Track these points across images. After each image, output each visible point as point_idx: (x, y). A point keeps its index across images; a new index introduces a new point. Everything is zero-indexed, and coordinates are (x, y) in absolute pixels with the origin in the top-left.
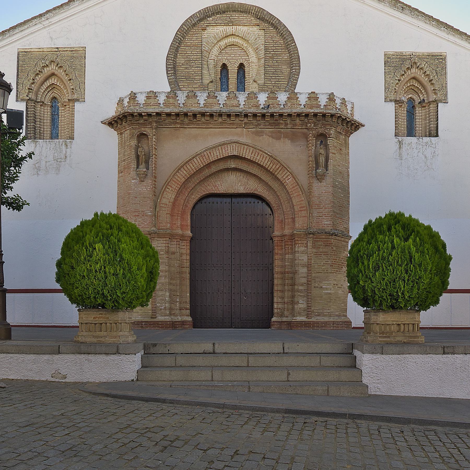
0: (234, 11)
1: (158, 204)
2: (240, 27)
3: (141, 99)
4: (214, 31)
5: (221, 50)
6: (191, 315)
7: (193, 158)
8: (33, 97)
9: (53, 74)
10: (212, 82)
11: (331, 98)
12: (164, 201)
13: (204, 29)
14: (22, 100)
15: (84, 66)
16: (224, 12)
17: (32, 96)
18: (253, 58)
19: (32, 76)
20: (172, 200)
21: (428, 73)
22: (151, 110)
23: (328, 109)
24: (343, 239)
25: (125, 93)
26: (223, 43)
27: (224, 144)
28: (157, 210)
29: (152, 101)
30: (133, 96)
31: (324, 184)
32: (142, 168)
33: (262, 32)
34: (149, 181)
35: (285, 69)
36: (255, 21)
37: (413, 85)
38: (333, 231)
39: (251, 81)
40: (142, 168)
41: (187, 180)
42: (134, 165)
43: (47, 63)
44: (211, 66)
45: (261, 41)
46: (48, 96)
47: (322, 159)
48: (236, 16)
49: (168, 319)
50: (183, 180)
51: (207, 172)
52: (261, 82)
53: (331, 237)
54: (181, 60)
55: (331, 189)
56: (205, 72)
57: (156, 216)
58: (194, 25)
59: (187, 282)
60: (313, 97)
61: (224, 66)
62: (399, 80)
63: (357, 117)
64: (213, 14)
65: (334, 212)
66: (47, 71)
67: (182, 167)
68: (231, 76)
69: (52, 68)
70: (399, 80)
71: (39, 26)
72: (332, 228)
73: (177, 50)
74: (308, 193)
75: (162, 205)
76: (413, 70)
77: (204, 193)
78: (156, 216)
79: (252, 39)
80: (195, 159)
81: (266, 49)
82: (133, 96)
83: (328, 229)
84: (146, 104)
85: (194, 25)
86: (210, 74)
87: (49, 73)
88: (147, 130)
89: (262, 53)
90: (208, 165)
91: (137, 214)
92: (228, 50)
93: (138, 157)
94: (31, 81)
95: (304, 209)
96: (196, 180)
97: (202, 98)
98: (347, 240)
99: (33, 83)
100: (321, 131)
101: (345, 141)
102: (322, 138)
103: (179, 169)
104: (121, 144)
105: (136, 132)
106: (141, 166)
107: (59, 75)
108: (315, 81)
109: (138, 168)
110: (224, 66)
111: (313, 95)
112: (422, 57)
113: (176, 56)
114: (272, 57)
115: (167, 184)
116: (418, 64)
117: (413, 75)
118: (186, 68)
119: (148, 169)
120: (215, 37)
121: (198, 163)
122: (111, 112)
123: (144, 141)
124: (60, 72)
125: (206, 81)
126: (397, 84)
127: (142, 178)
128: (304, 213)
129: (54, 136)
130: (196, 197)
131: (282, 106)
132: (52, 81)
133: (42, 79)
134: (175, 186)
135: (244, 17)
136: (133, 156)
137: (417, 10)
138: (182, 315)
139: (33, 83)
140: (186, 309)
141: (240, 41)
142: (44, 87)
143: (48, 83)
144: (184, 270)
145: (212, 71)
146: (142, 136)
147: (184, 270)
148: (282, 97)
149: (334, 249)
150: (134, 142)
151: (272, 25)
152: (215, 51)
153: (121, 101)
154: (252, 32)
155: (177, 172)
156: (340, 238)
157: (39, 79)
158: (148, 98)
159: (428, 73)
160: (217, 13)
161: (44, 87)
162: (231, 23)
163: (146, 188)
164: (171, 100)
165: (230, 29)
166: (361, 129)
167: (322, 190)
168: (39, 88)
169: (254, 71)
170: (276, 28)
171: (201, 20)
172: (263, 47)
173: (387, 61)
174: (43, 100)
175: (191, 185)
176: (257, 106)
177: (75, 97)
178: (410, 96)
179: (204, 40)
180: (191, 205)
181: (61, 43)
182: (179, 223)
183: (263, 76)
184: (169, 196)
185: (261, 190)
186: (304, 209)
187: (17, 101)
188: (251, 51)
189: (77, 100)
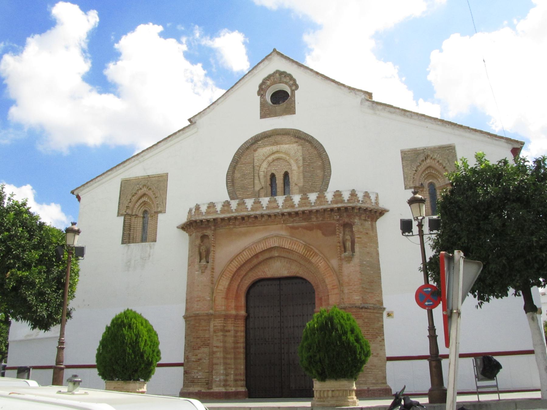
0: (278, 134)
1: (215, 291)
2: (283, 146)
3: (204, 209)
4: (263, 151)
5: (269, 164)
6: (247, 386)
7: (243, 251)
8: (130, 212)
9: (144, 195)
10: (262, 188)
11: (353, 194)
12: (220, 287)
13: (255, 150)
14: (122, 215)
15: (166, 187)
16: (270, 136)
17: (129, 212)
18: (294, 167)
19: (130, 197)
20: (226, 286)
21: (441, 161)
22: (210, 217)
23: (351, 203)
24: (375, 311)
25: (193, 206)
26: (270, 159)
27: (267, 238)
28: (214, 295)
29: (212, 210)
30: (198, 208)
31: (352, 264)
32: (203, 262)
33: (300, 147)
34: (208, 272)
35: (319, 172)
36: (294, 140)
37: (430, 172)
38: (363, 305)
39: (294, 184)
40: (203, 262)
41: (239, 269)
42: (197, 260)
43: (141, 187)
44: (261, 177)
45: (300, 154)
46: (140, 211)
47: (348, 244)
48: (279, 138)
49: (223, 390)
50: (235, 269)
51: (255, 261)
52: (301, 184)
53: (361, 310)
54: (237, 175)
55: (358, 269)
56: (257, 181)
57: (213, 300)
58: (248, 148)
59: (242, 356)
60: (338, 194)
61: (273, 176)
62: (416, 171)
63: (382, 204)
64: (262, 139)
65: (363, 288)
66: (140, 193)
67: (234, 259)
68: (279, 183)
69: (144, 190)
70: (416, 171)
71: (137, 162)
72: (361, 302)
73: (235, 168)
74: (338, 274)
75: (218, 291)
76: (428, 161)
77: (255, 278)
78: (213, 300)
79: (292, 153)
80: (244, 252)
81: (304, 159)
82: (198, 208)
83: (359, 303)
84: (207, 213)
85: (248, 148)
86: (262, 182)
87: (142, 194)
88: (209, 232)
89: (301, 163)
90: (257, 256)
91: (198, 299)
92: (275, 163)
93: (200, 254)
94: (129, 201)
95: (335, 287)
96: (247, 268)
97: (249, 203)
98: (381, 312)
99: (130, 202)
100: (346, 220)
101: (372, 225)
102: (348, 226)
103: (232, 261)
104: (191, 243)
105: (200, 234)
106: (202, 261)
107: (149, 194)
108: (346, 179)
109: (200, 262)
110: (273, 176)
111: (337, 193)
112: (434, 150)
113: (234, 172)
114: (308, 165)
115: (222, 273)
116: (431, 156)
117: (428, 165)
118: (242, 180)
119: (208, 262)
120: (264, 155)
121: (247, 255)
122: (184, 219)
123: (206, 241)
124: (150, 193)
125: (257, 188)
126: (415, 174)
127: (203, 270)
128: (336, 291)
129: (144, 239)
130: (248, 282)
131: (313, 204)
132: (145, 199)
133: (137, 199)
134: (229, 275)
135: (286, 138)
136: (197, 253)
137: (423, 115)
138: (236, 386)
139: (130, 202)
140: (241, 380)
141: (284, 156)
142: (139, 203)
143: (141, 201)
144: (239, 345)
145: (262, 180)
146: (204, 237)
147: (239, 345)
148: (313, 197)
149: (366, 320)
150: (198, 242)
151: (308, 141)
152: (265, 165)
153: (190, 210)
154: (292, 149)
155: (231, 263)
156: (372, 311)
157: (134, 199)
158: (209, 207)
159: (441, 161)
160: (265, 137)
161: (139, 203)
162: (276, 143)
163: (205, 279)
164: (226, 208)
165: (275, 148)
166: (386, 215)
167: (351, 270)
168: (135, 205)
169: (295, 177)
170: (310, 142)
171: (252, 144)
172: (301, 158)
173: (405, 157)
174: (137, 213)
175: (243, 273)
176: (293, 206)
177: (159, 209)
178: (430, 181)
179: (256, 158)
180: (244, 288)
181: (150, 173)
182: (233, 305)
183: (302, 180)
184: (224, 283)
185: (301, 273)
186: (335, 287)
187: (118, 216)
188: (292, 162)
189: (161, 212)
